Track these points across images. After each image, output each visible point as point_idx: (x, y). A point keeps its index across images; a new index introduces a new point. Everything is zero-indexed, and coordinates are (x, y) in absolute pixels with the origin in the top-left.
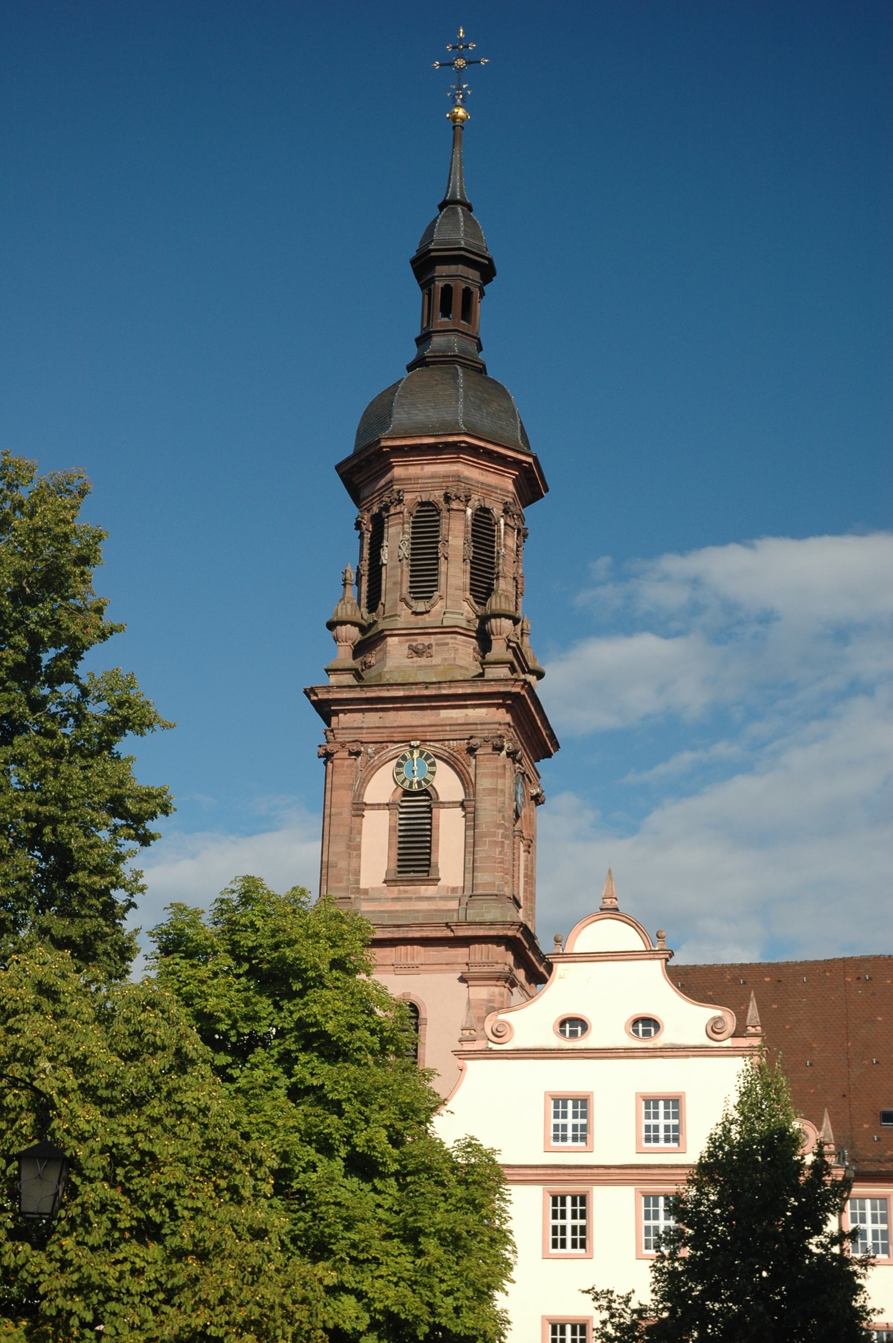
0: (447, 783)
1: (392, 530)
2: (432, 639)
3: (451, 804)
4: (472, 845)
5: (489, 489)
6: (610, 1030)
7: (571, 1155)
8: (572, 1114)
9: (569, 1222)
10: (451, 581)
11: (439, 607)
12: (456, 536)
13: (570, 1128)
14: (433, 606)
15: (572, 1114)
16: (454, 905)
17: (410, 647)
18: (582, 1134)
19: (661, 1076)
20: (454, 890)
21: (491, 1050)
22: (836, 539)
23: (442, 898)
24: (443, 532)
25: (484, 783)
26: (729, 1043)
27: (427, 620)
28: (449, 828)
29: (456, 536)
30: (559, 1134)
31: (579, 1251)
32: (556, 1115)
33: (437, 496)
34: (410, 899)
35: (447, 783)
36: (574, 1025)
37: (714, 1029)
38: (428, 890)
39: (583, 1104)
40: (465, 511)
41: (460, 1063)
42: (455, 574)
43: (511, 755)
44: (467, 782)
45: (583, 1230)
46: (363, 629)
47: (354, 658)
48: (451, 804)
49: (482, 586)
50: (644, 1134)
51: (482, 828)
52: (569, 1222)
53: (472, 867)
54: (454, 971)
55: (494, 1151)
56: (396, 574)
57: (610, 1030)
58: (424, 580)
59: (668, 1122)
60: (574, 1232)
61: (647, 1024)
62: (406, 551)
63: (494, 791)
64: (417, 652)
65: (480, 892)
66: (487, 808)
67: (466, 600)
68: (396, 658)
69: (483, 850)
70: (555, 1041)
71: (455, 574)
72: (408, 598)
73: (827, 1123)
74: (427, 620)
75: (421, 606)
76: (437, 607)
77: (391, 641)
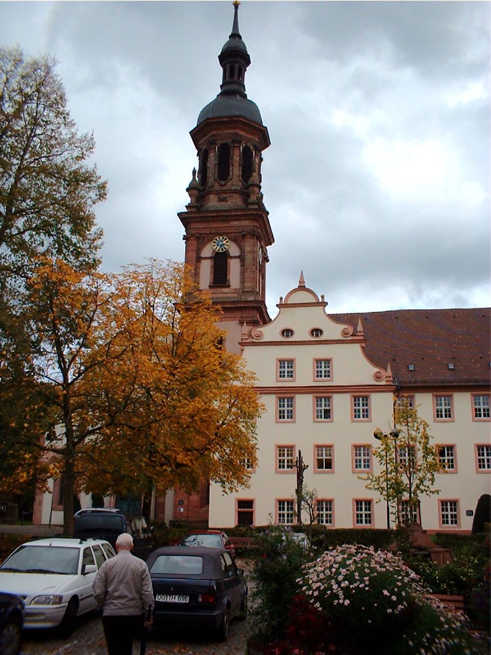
0: (234, 250)
1: (211, 154)
2: (227, 195)
3: (235, 257)
4: (243, 273)
5: (249, 140)
6: (302, 334)
7: (286, 383)
8: (286, 366)
9: (362, 458)
10: (235, 173)
12: (236, 157)
13: (323, 372)
14: (228, 182)
15: (286, 366)
16: (235, 295)
17: (219, 198)
18: (291, 374)
19: (323, 352)
20: (236, 290)
21: (254, 342)
23: (231, 293)
24: (231, 154)
26: (350, 338)
27: (226, 188)
28: (234, 267)
29: (236, 157)
30: (282, 375)
31: (290, 420)
32: (281, 367)
33: (229, 141)
34: (218, 293)
35: (234, 250)
36: (287, 332)
37: (345, 333)
38: (226, 290)
39: (291, 362)
40: (240, 147)
41: (242, 348)
42: (236, 171)
46: (200, 191)
47: (197, 202)
48: (235, 257)
50: (316, 374)
51: (247, 266)
53: (243, 281)
54: (236, 320)
57: (302, 334)
59: (325, 369)
60: (365, 462)
61: (317, 332)
64: (220, 200)
65: (246, 290)
67: (241, 181)
69: (247, 274)
71: (236, 171)
72: (218, 180)
73: (389, 370)
74: (226, 188)
75: (223, 183)
76: (229, 183)
77: (212, 196)
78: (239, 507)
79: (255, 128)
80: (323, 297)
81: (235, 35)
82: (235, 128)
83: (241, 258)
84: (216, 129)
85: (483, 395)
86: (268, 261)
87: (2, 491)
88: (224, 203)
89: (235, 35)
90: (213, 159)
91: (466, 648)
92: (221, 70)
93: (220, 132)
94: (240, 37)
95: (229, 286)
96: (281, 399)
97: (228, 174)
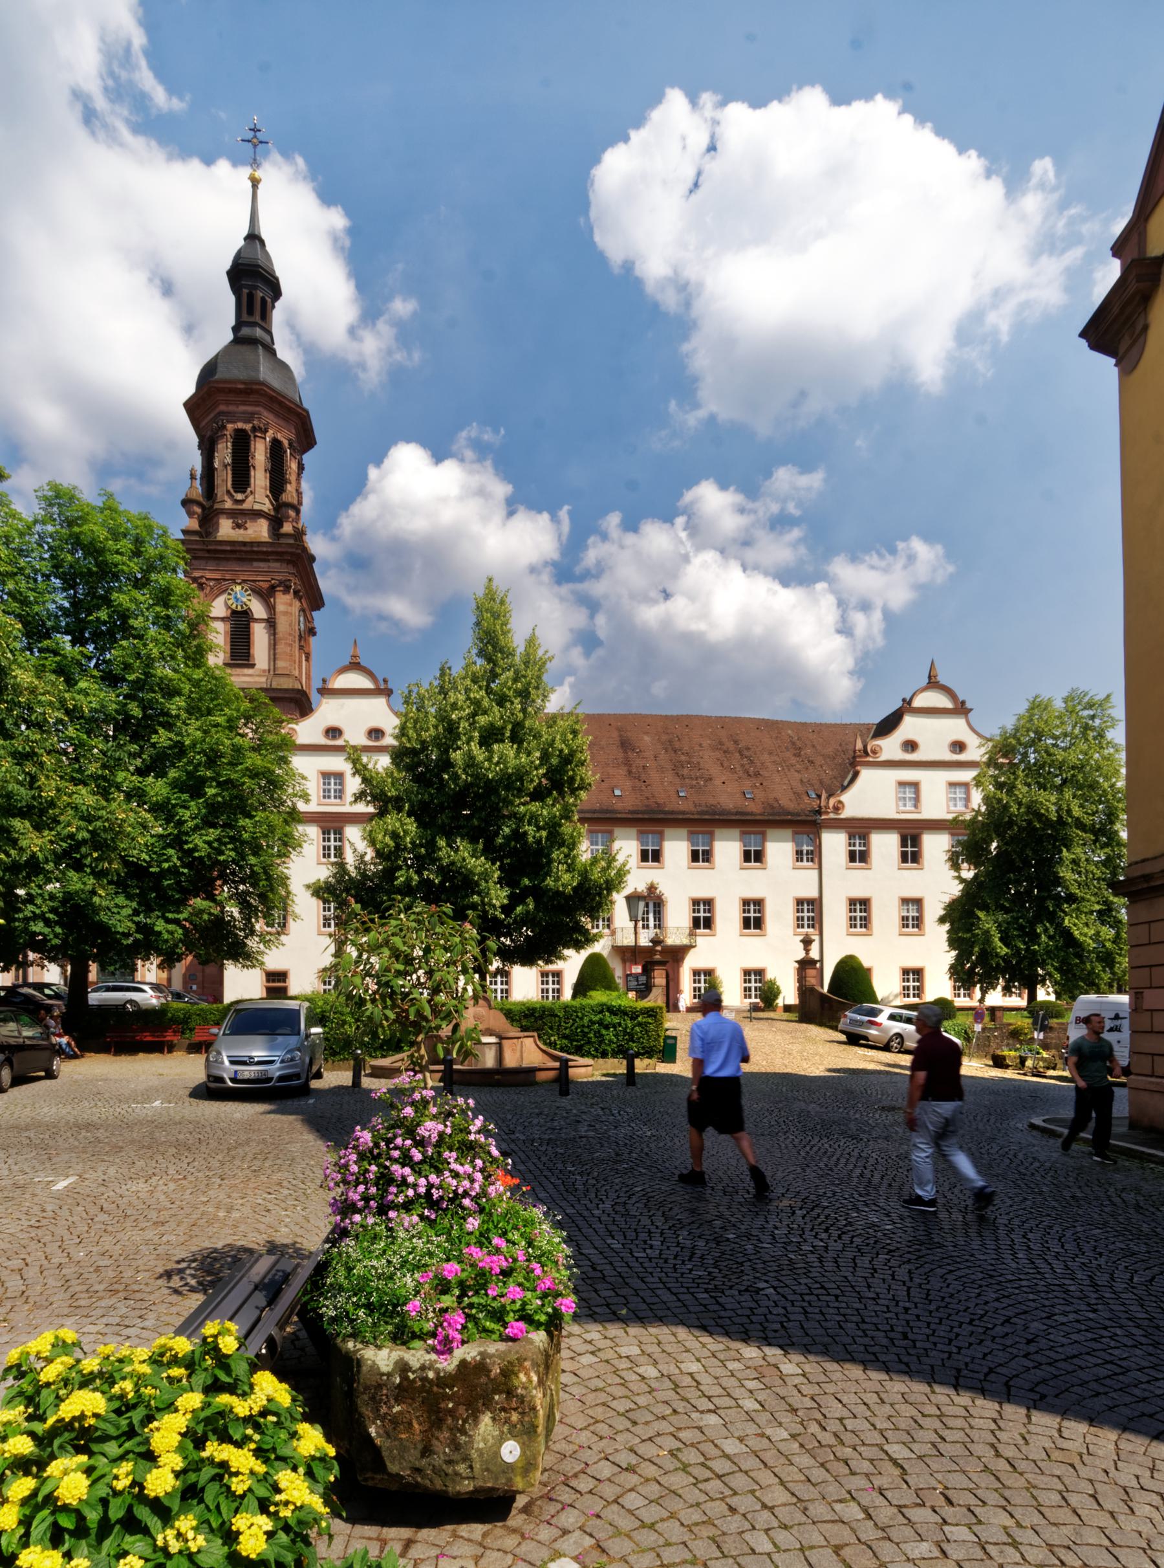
0: (258, 609)
11: (251, 498)
12: (260, 453)
22: (129, 1058)
25: (280, 608)
28: (259, 634)
35: (258, 609)
42: (260, 479)
43: (296, 593)
44: (271, 608)
45: (558, 991)
49: (277, 483)
51: (279, 635)
52: (551, 986)
53: (274, 657)
55: (296, 917)
56: (224, 479)
58: (242, 481)
62: (229, 460)
63: (286, 613)
66: (282, 624)
68: (226, 529)
69: (281, 648)
70: (323, 741)
71: (260, 479)
74: (246, 506)
75: (239, 496)
78: (268, 981)
79: (289, 409)
80: (385, 681)
81: (254, 237)
82: (257, 404)
83: (271, 623)
84: (228, 403)
85: (602, 832)
86: (314, 634)
87: (11, 991)
88: (242, 531)
89: (254, 237)
90: (224, 453)
91: (78, 984)
92: (232, 299)
93: (232, 408)
94: (262, 242)
95: (253, 666)
96: (326, 832)
97: (248, 485)
